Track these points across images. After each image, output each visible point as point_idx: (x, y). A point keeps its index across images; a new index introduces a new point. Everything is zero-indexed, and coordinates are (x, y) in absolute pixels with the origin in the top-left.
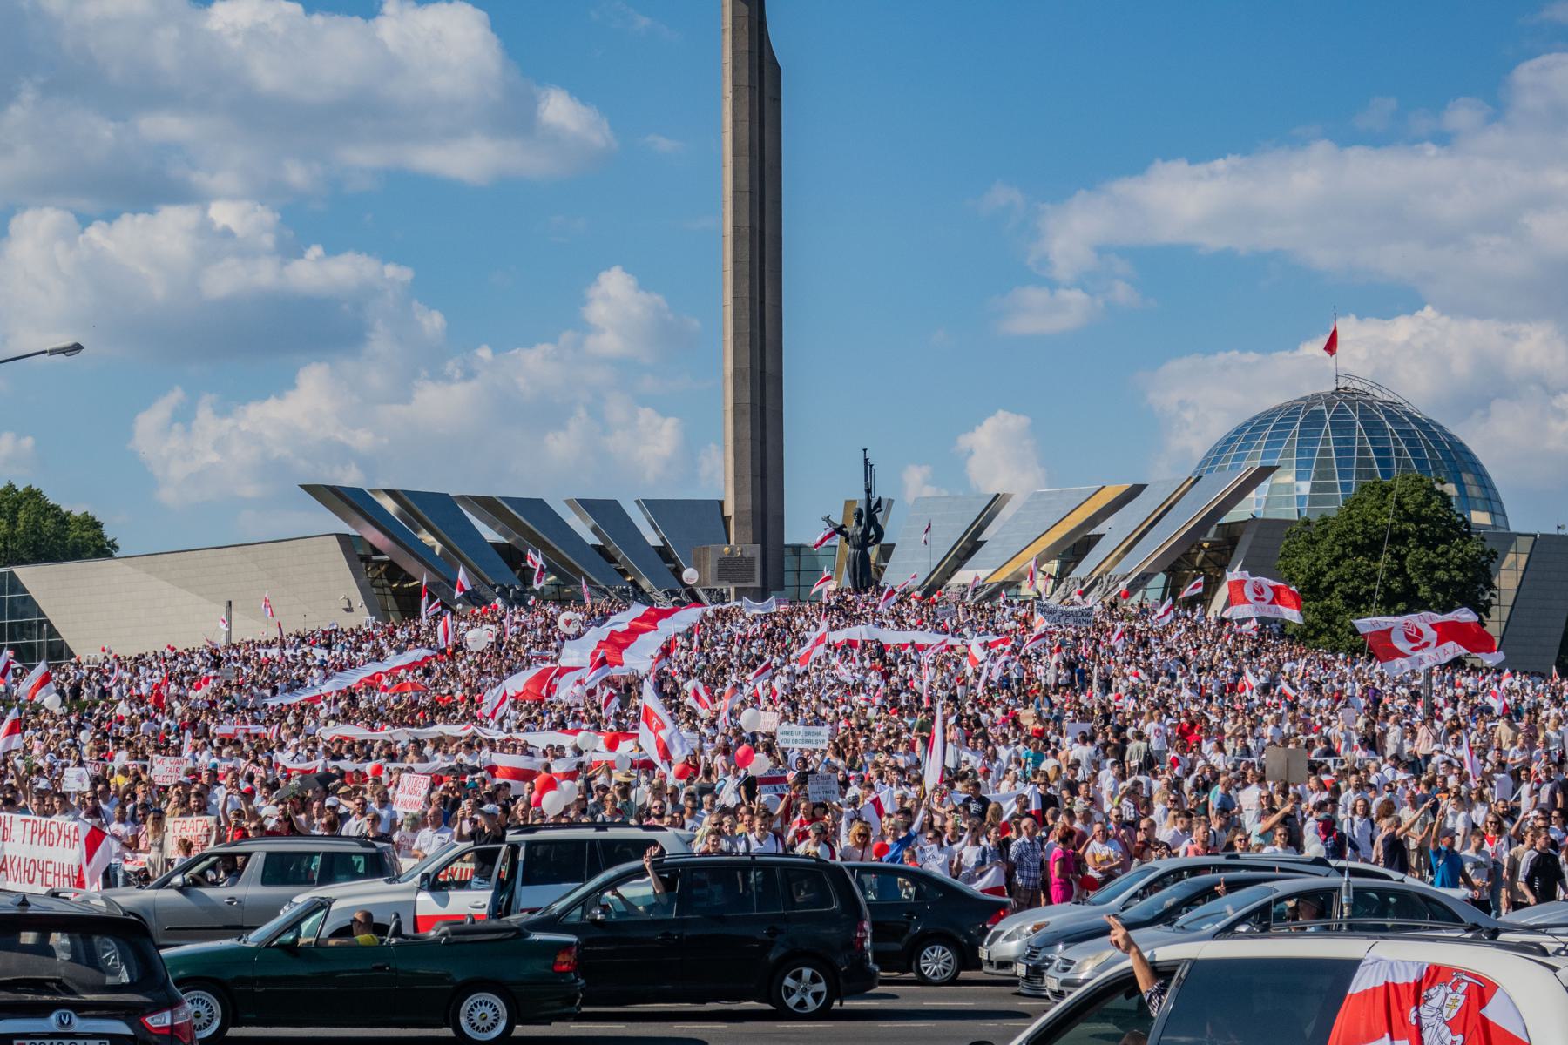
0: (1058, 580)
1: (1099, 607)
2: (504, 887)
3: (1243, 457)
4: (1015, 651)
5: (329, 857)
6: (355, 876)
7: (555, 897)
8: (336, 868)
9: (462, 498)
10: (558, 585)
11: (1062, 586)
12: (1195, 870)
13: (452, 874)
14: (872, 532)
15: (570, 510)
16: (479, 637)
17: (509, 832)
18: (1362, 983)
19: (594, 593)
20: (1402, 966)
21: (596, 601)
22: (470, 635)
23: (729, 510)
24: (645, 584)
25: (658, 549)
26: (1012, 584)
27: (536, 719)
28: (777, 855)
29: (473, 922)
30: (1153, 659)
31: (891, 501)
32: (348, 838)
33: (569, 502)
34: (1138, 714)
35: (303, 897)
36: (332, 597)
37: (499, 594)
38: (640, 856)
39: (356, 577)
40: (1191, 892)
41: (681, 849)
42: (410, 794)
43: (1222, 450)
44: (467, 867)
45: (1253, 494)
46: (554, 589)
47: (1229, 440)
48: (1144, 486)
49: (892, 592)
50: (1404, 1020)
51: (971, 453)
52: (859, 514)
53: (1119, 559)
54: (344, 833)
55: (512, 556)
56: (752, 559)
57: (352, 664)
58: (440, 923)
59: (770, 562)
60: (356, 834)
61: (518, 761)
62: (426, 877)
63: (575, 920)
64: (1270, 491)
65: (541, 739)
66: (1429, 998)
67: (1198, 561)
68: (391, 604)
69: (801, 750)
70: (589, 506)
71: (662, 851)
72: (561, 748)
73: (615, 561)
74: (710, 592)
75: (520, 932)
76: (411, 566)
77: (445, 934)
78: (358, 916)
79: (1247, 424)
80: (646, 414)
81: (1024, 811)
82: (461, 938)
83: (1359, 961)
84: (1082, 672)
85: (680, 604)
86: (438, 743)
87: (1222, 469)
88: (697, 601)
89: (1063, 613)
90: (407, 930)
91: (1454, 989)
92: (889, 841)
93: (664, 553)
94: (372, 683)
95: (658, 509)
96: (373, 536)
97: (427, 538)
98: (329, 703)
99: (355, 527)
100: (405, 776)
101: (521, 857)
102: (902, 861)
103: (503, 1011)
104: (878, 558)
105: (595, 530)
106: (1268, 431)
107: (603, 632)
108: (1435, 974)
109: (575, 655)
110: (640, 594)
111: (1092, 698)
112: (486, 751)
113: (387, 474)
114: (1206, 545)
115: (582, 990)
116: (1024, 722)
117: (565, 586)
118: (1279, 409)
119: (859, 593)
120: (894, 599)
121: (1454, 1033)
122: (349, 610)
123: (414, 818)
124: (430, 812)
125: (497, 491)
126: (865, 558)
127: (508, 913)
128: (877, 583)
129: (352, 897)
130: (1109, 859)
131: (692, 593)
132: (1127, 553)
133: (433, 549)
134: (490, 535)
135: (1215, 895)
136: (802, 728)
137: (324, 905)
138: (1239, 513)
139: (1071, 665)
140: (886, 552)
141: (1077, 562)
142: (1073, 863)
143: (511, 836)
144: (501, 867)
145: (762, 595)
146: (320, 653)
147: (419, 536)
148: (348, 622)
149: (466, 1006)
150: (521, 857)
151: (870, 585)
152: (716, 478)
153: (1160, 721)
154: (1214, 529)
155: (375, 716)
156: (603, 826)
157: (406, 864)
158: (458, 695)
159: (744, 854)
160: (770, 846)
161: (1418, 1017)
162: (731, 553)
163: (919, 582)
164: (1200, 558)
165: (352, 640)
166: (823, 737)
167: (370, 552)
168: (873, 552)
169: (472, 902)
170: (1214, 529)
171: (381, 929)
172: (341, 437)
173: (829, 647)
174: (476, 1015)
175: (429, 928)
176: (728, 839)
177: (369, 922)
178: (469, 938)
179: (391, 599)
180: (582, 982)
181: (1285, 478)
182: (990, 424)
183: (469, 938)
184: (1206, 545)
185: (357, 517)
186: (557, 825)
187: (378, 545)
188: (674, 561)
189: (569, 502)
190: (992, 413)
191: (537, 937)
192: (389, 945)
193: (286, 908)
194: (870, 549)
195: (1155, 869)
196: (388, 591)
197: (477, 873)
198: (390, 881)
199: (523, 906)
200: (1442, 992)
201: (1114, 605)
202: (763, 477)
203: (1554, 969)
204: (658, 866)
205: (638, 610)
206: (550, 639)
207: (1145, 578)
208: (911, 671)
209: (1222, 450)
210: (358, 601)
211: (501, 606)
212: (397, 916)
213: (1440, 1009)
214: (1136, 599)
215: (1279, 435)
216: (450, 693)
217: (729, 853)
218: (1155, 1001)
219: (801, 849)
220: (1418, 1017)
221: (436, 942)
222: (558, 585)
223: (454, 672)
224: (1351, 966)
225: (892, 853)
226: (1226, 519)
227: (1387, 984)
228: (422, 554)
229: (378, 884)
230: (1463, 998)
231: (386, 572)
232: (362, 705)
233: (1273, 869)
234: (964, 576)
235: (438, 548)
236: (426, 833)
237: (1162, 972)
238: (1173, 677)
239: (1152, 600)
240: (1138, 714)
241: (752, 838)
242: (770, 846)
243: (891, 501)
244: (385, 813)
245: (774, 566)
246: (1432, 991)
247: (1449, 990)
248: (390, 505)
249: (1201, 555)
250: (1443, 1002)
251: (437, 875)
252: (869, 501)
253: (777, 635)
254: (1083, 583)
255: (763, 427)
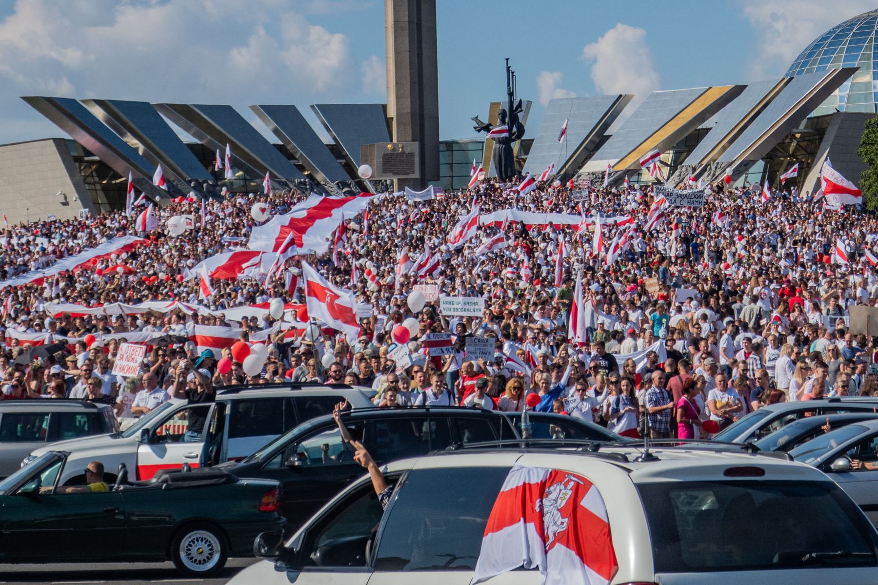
0: (673, 168)
1: (708, 191)
2: (213, 441)
3: (827, 61)
4: (638, 229)
5: (57, 418)
6: (80, 432)
7: (258, 447)
8: (63, 426)
9: (162, 106)
10: (245, 179)
11: (677, 173)
12: (800, 413)
13: (167, 430)
14: (515, 130)
15: (254, 114)
16: (177, 225)
17: (218, 392)
18: (510, 483)
19: (277, 186)
20: (535, 470)
21: (278, 192)
22: (172, 221)
23: (392, 112)
24: (320, 177)
25: (330, 147)
26: (634, 172)
27: (229, 295)
28: (450, 407)
29: (189, 470)
30: (756, 233)
31: (529, 103)
32: (75, 400)
33: (253, 108)
34: (745, 281)
35: (41, 452)
36: (54, 193)
37: (194, 188)
38: (330, 410)
39: (72, 176)
40: (802, 431)
41: (364, 404)
42: (129, 361)
43: (810, 55)
44: (180, 424)
45: (837, 92)
46: (242, 183)
47: (816, 47)
48: (745, 87)
49: (533, 180)
50: (533, 509)
51: (595, 60)
52: (503, 114)
53: (724, 149)
54: (72, 396)
55: (204, 155)
56: (412, 155)
57: (70, 252)
58: (160, 471)
59: (427, 155)
60: (82, 396)
61: (217, 331)
62: (146, 432)
63: (276, 467)
64: (851, 89)
65: (234, 314)
66: (550, 493)
67: (791, 149)
68: (101, 198)
69: (462, 318)
70: (272, 111)
71: (349, 406)
72: (254, 319)
73: (293, 158)
74: (376, 183)
75: (230, 478)
76: (119, 165)
77: (165, 481)
78: (91, 467)
79: (830, 32)
80: (316, 32)
81: (655, 365)
82: (179, 484)
83: (511, 468)
84: (696, 246)
85: (353, 195)
86: (149, 316)
87: (810, 71)
88: (366, 192)
89: (679, 196)
90: (132, 478)
91: (566, 486)
92: (541, 394)
93: (335, 150)
94: (85, 268)
95: (331, 113)
96: (86, 140)
97: (132, 141)
98: (51, 285)
99: (69, 132)
100: (124, 346)
101: (228, 411)
102: (552, 411)
103: (217, 546)
104: (520, 150)
105: (276, 132)
106: (849, 38)
107: (286, 219)
108: (555, 476)
109: (262, 240)
110: (316, 186)
111: (705, 267)
112: (190, 324)
113: (95, 86)
114: (798, 136)
115: (284, 527)
116: (650, 289)
117: (251, 180)
118: (858, 19)
119: (505, 182)
120: (533, 186)
121: (563, 517)
122: (65, 204)
123: (133, 382)
124: (145, 377)
125: (191, 99)
126: (509, 151)
127: (217, 462)
128: (520, 173)
129: (84, 450)
130: (728, 404)
131: (360, 184)
132: (732, 142)
133: (137, 149)
134: (186, 137)
135: (822, 432)
136: (461, 299)
137: (60, 458)
138: (825, 109)
139: (686, 240)
140: (527, 146)
141: (689, 152)
142: (692, 412)
143: (220, 396)
144: (210, 424)
145: (421, 184)
146: (42, 241)
147: (125, 139)
148: (66, 214)
149: (184, 543)
150: (228, 411)
151: (513, 175)
152: (380, 84)
153: (765, 286)
154: (804, 122)
155: (90, 295)
156: (297, 385)
157: (126, 422)
158: (162, 276)
159: (419, 407)
160: (444, 400)
161: (541, 507)
162: (394, 149)
163: (555, 171)
164: (791, 149)
165: (69, 229)
166: (478, 307)
167: (82, 153)
168: (516, 146)
169: (186, 453)
170: (804, 122)
171: (110, 478)
172: (54, 54)
173: (479, 228)
174: (194, 550)
175: (152, 476)
176: (403, 394)
177: (101, 472)
178: (186, 484)
179: (101, 193)
180: (284, 519)
181: (864, 77)
182: (611, 36)
183: (186, 484)
184: (798, 136)
185: (71, 124)
186: (256, 386)
187: (89, 147)
188: (345, 157)
189: (253, 108)
190: (613, 26)
191: (244, 482)
192: (117, 491)
193: (26, 461)
194: (512, 144)
195: (769, 413)
196: (98, 187)
197: (189, 428)
198: (115, 436)
199: (229, 456)
200: (558, 490)
201: (720, 189)
202: (421, 84)
203: (629, 471)
204: (346, 418)
205: (314, 200)
206: (242, 226)
207: (744, 167)
208: (550, 248)
209: (810, 55)
210: (73, 196)
211: (195, 198)
212: (124, 466)
213: (556, 501)
214: (740, 183)
215: (858, 41)
216: (155, 274)
217: (404, 407)
218: (386, 501)
219: (467, 401)
220: (541, 507)
221: (158, 488)
222: (245, 179)
223: (159, 257)
224: (503, 473)
225: (544, 403)
226: (813, 114)
227: (524, 484)
228: (128, 154)
229: (105, 439)
230: (570, 493)
231: (96, 170)
232: (78, 286)
233: (871, 410)
234: (595, 165)
235: (141, 149)
236: (143, 394)
237: (390, 480)
238: (774, 248)
239: (753, 183)
240: (745, 281)
241: (429, 392)
242: (444, 400)
243: (529, 103)
244: (106, 378)
245: (430, 160)
246: (552, 488)
247: (562, 487)
248: (99, 113)
249: (794, 144)
250: (559, 495)
251: (155, 430)
252: (511, 103)
253: (434, 219)
254: (694, 170)
255: (420, 42)
